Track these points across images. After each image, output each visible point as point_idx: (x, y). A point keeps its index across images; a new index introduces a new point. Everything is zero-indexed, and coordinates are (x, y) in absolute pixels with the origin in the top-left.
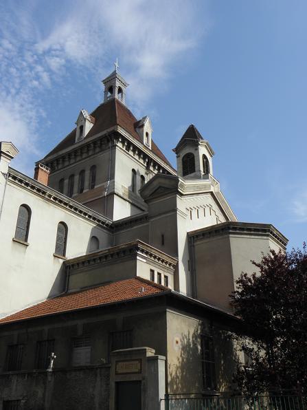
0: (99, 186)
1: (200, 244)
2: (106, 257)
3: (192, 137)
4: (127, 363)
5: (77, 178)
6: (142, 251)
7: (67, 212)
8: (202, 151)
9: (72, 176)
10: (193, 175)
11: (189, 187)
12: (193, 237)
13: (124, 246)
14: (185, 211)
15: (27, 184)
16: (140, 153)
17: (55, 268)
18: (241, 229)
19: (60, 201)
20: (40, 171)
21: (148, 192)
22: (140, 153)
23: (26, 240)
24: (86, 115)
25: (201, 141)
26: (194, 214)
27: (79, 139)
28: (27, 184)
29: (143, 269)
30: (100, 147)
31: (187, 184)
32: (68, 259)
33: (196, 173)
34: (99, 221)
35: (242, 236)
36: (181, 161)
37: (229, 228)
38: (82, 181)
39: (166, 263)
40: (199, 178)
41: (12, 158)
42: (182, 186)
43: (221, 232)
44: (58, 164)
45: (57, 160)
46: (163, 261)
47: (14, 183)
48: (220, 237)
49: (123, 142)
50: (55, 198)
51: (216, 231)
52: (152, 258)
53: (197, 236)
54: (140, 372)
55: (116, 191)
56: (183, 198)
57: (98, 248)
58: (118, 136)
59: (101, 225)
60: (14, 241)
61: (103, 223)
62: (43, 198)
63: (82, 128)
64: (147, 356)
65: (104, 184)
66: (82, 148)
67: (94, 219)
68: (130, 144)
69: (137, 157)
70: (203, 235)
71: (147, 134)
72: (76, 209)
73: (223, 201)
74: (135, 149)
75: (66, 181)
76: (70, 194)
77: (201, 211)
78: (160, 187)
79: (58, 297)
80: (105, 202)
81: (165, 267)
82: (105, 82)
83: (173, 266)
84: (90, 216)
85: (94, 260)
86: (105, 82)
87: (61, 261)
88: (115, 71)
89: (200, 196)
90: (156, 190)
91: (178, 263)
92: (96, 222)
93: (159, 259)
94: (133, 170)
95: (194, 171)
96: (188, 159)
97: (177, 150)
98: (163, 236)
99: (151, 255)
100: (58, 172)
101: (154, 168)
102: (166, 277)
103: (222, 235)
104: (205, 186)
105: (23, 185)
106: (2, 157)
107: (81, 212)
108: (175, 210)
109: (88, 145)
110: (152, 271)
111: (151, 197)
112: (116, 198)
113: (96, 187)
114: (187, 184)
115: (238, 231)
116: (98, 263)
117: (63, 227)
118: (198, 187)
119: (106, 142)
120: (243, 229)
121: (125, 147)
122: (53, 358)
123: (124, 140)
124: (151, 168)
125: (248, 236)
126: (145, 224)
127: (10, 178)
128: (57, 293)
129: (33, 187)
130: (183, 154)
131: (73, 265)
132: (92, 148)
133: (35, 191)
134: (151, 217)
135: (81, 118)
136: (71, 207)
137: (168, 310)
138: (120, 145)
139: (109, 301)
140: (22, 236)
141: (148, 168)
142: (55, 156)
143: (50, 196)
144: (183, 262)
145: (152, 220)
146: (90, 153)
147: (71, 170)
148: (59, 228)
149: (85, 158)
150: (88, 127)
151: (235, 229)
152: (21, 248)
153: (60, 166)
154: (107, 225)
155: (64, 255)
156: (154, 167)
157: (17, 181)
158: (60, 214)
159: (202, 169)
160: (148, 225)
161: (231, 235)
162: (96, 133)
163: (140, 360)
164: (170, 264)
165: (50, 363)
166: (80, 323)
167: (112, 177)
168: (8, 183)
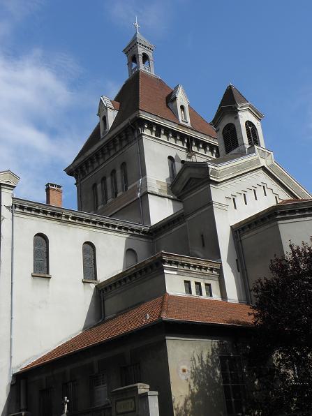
0: (133, 185)
1: (248, 238)
2: (135, 275)
3: (229, 103)
4: (124, 402)
5: (109, 180)
6: (170, 262)
7: (91, 229)
8: (245, 116)
9: (104, 179)
10: (236, 151)
11: (225, 171)
12: (238, 231)
13: (149, 261)
14: (224, 201)
15: (38, 211)
16: (175, 134)
17: (83, 297)
18: (290, 212)
19: (81, 220)
20: (51, 191)
21: (179, 187)
22: (175, 134)
23: (48, 273)
24: (107, 102)
25: (240, 105)
26: (237, 199)
27: (103, 134)
28: (38, 211)
29: (174, 284)
30: (127, 139)
31: (221, 170)
32: (101, 281)
33: (240, 148)
34: (132, 230)
35: (295, 220)
36: (222, 136)
37: (276, 214)
38: (114, 182)
39: (206, 269)
40: (242, 154)
41: (14, 187)
42: (215, 172)
43: (268, 220)
44: (87, 167)
45: (85, 162)
46: (200, 268)
47: (23, 213)
48: (268, 226)
49: (150, 128)
50: (73, 218)
51: (262, 220)
52: (185, 268)
53: (243, 229)
54: (134, 411)
55: (149, 190)
56: (219, 186)
57: (137, 261)
58: (142, 122)
59: (135, 233)
60: (33, 276)
61: (138, 231)
62: (59, 220)
63: (105, 119)
64: (139, 393)
65: (136, 183)
66: (107, 144)
67: (126, 229)
68: (159, 128)
69: (172, 141)
70: (249, 226)
71: (182, 107)
72: (101, 224)
73: (282, 174)
74: (168, 131)
75: (99, 186)
76: (95, 209)
77: (250, 196)
78: (191, 179)
79: (95, 326)
80: (140, 205)
81: (204, 274)
82: (127, 51)
83: (216, 270)
84: (120, 228)
85: (125, 280)
86: (127, 51)
87: (93, 286)
88: (135, 38)
89: (246, 176)
90: (187, 183)
91: (221, 267)
92: (129, 232)
93: (195, 267)
94: (170, 158)
95: (237, 146)
96: (229, 131)
97: (215, 123)
98: (202, 236)
99: (183, 265)
100: (89, 177)
101: (198, 148)
102: (208, 285)
103: (269, 223)
104: (251, 163)
105: (33, 213)
106: (3, 190)
107: (108, 225)
108: (209, 203)
109: (113, 140)
110: (187, 283)
111: (183, 193)
112: (151, 199)
113: (129, 188)
114: (221, 170)
115: (288, 216)
116: (129, 283)
117: (89, 248)
118: (239, 167)
119: (131, 132)
120: (294, 212)
121: (154, 134)
122: (66, 402)
123: (151, 125)
124: (194, 149)
125: (302, 219)
126: (183, 225)
127: (17, 209)
128: (93, 322)
129: (45, 212)
130: (221, 127)
131: (106, 289)
132: (118, 142)
133: (48, 216)
134: (188, 216)
135: (102, 110)
136: (95, 222)
137: (167, 338)
138: (147, 132)
139: (115, 334)
140: (42, 268)
141: (189, 150)
142: (82, 159)
143: (67, 217)
144: (228, 261)
145: (188, 219)
146: (118, 148)
147: (102, 175)
148: (84, 250)
149: (113, 156)
150: (112, 116)
151: (284, 213)
152: (44, 282)
153: (90, 170)
154: (143, 232)
155: (96, 279)
156: (197, 145)
157: (25, 211)
158: (84, 233)
159: (246, 141)
160: (186, 226)
161: (279, 222)
162: (122, 122)
163: (134, 398)
164: (211, 269)
165: (64, 408)
166: (95, 359)
167: (143, 173)
168: (15, 214)
